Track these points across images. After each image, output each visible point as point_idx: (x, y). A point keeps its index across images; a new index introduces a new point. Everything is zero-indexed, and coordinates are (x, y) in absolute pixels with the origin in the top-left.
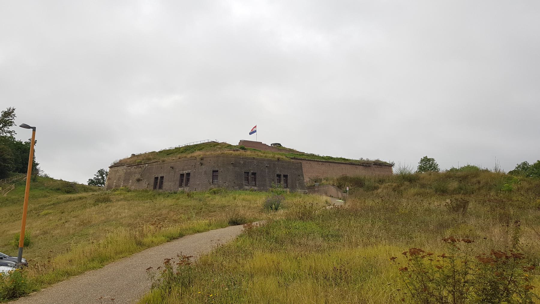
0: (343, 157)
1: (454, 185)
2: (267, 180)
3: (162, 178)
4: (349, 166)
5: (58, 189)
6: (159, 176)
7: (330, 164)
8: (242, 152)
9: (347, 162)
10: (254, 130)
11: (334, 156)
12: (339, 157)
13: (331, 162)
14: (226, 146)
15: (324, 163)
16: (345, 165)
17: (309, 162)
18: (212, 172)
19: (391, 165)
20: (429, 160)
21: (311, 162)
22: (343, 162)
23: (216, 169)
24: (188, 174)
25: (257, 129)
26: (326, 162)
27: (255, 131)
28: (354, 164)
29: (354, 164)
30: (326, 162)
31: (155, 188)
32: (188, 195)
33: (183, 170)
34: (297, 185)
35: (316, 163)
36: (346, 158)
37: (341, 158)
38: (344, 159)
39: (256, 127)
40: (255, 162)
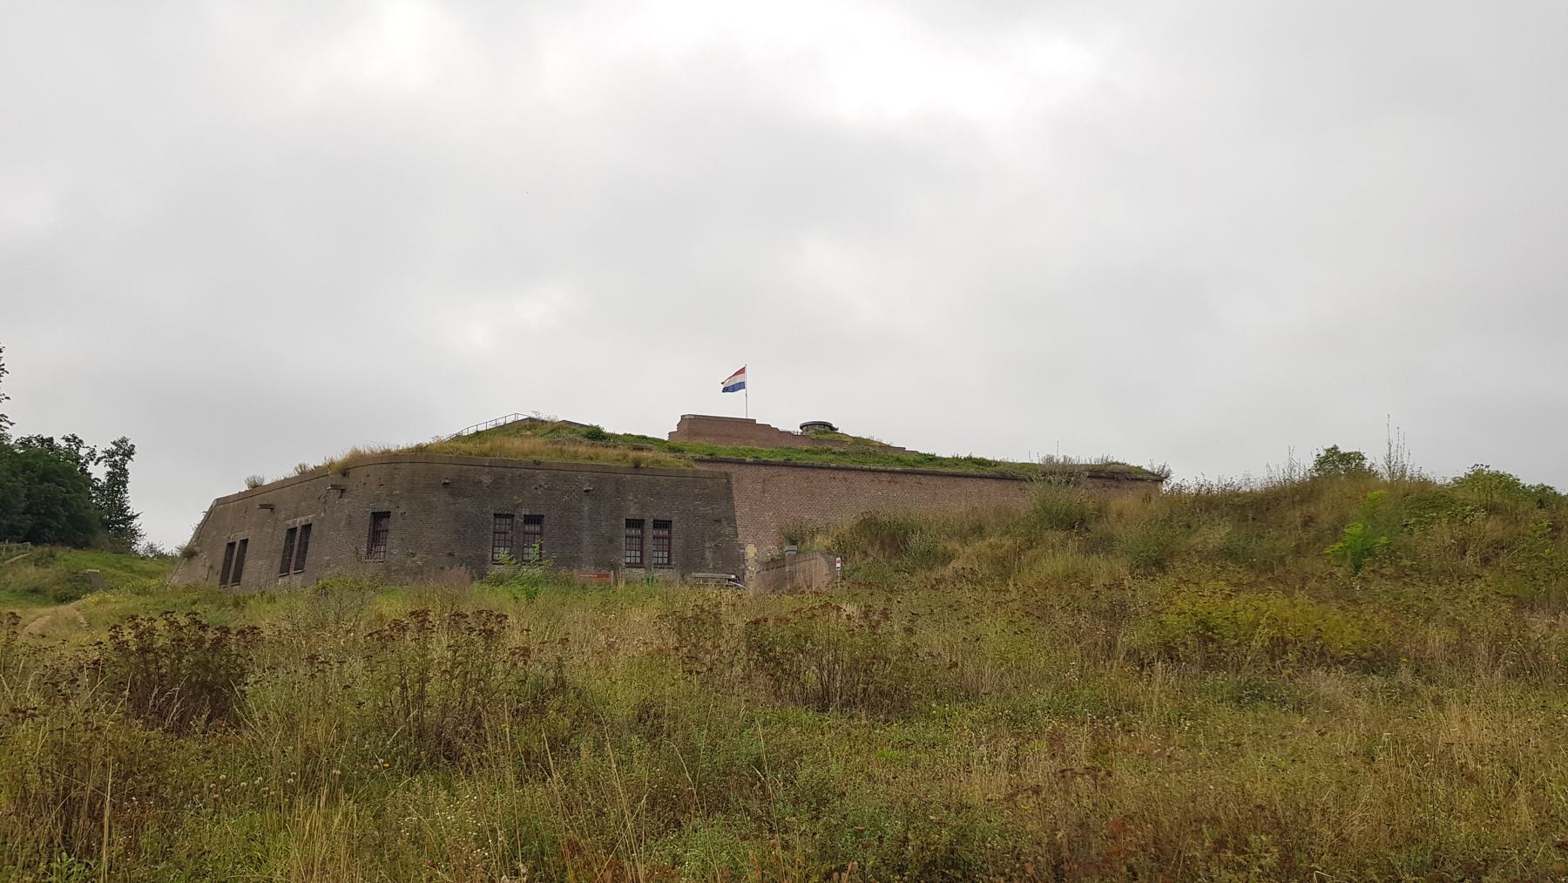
0: (976, 455)
1: (1217, 534)
2: (586, 538)
3: (245, 542)
4: (995, 484)
5: (35, 591)
6: (238, 537)
7: (923, 480)
8: (668, 457)
9: (988, 471)
10: (739, 379)
11: (945, 453)
12: (964, 455)
13: (813, 467)
14: (550, 427)
15: (900, 478)
16: (981, 482)
17: (841, 475)
18: (368, 517)
19: (1158, 478)
20: (1347, 458)
21: (851, 476)
22: (972, 470)
23: (384, 506)
24: (307, 528)
25: (748, 378)
26: (905, 473)
27: (741, 386)
28: (1014, 479)
29: (1014, 479)
30: (905, 473)
31: (224, 581)
32: (236, 604)
33: (296, 516)
34: (708, 554)
35: (871, 476)
36: (989, 458)
37: (970, 460)
38: (982, 463)
39: (742, 371)
40: (542, 476)
